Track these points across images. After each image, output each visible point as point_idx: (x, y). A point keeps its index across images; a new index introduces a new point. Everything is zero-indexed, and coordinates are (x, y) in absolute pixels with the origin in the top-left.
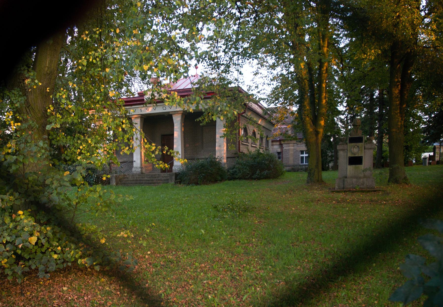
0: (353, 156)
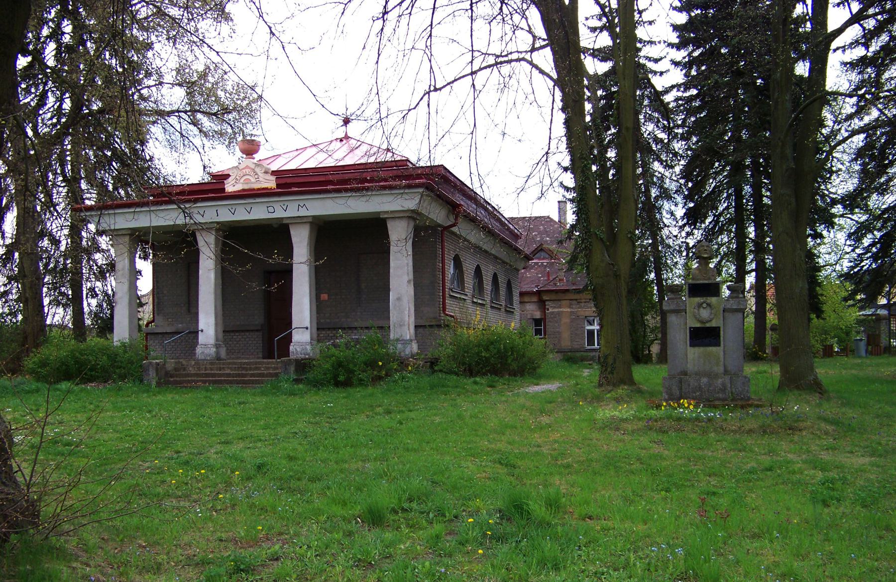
0: (698, 325)
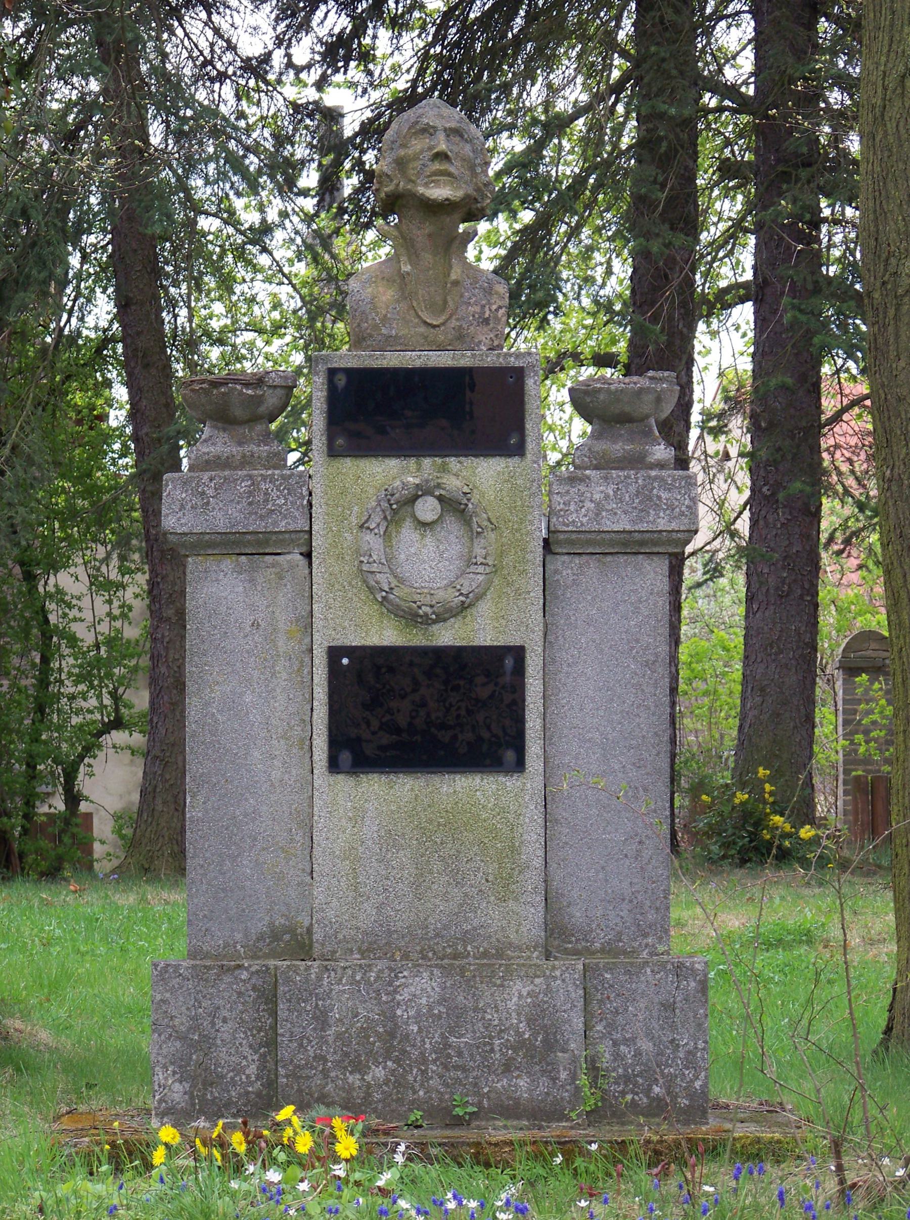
0: (387, 635)
